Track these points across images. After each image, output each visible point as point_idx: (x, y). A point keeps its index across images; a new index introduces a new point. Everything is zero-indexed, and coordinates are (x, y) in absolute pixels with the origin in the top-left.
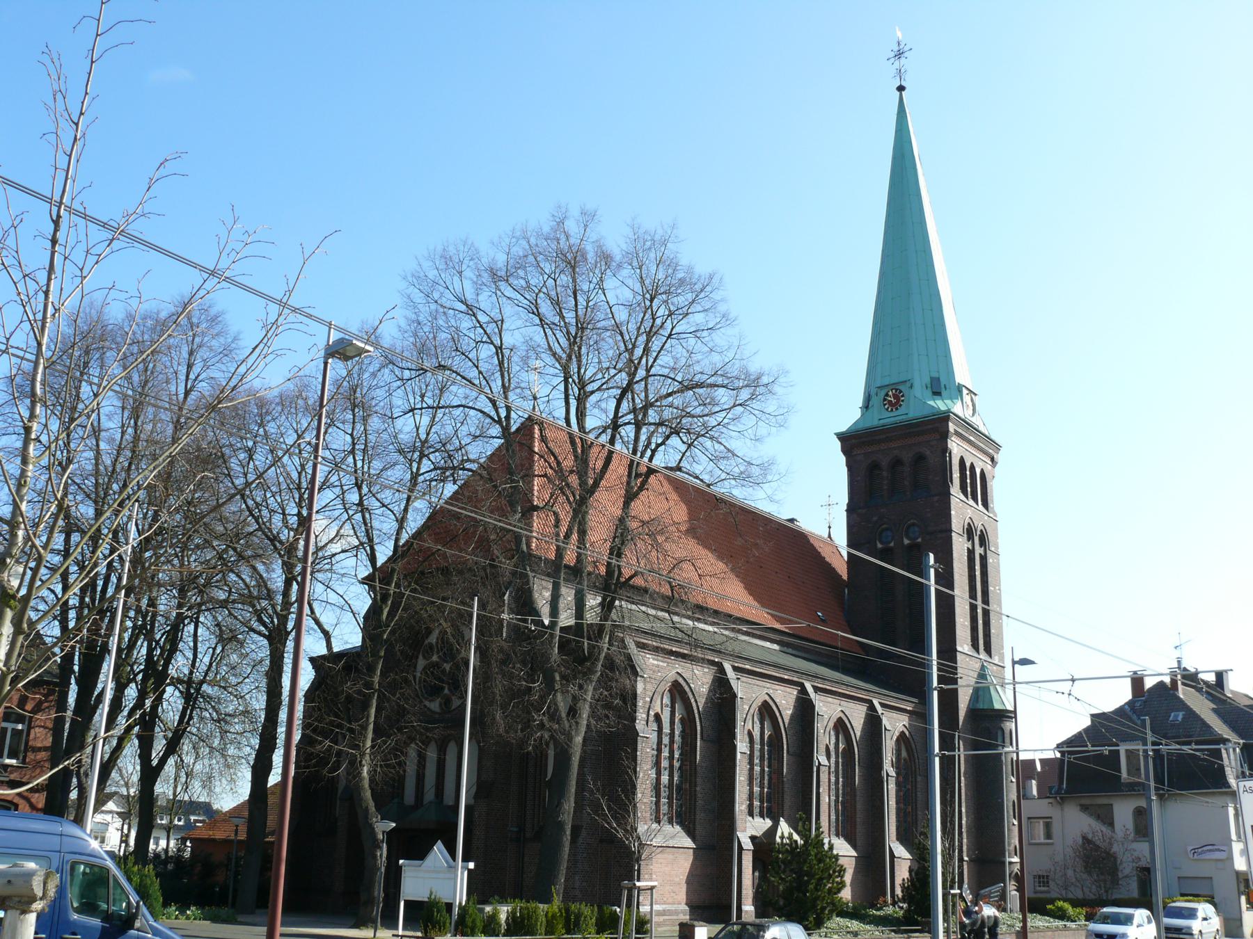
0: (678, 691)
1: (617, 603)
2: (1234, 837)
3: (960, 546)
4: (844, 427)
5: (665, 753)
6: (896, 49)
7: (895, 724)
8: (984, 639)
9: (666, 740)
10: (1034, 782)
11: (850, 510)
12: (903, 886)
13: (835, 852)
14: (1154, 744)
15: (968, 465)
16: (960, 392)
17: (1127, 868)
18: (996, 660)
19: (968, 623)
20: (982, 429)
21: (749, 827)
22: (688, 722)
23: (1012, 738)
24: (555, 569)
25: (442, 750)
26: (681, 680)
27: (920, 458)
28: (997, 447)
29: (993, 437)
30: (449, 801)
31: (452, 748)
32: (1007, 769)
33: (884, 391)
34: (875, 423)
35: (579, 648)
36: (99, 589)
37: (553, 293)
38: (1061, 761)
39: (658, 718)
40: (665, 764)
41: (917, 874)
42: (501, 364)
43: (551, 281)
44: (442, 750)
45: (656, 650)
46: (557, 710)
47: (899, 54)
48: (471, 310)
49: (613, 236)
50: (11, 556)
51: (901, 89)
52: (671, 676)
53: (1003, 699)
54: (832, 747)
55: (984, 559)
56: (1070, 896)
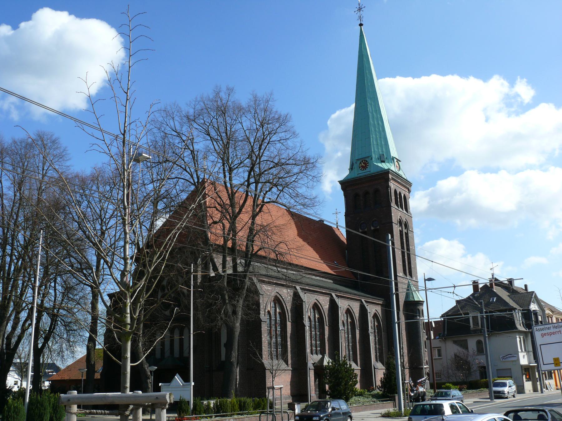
0: (278, 301)
1: (252, 263)
2: (520, 350)
3: (396, 229)
4: (342, 178)
5: (273, 328)
6: (358, 7)
7: (373, 309)
8: (409, 269)
9: (273, 323)
10: (432, 332)
11: (346, 215)
12: (381, 381)
13: (352, 368)
14: (486, 312)
15: (398, 193)
16: (394, 160)
17: (475, 368)
18: (414, 279)
19: (401, 263)
20: (403, 176)
21: (312, 359)
22: (283, 314)
23: (421, 313)
24: (222, 249)
25: (181, 334)
26: (278, 295)
27: (377, 191)
28: (410, 184)
29: (408, 180)
30: (185, 355)
31: (186, 331)
32: (421, 327)
33: (360, 160)
34: (356, 175)
35: (236, 283)
36: (7, 268)
37: (216, 126)
38: (444, 320)
39: (269, 312)
40: (273, 333)
41: (387, 375)
42: (194, 158)
43: (214, 120)
44: (181, 334)
45: (269, 283)
46: (228, 312)
47: (360, 9)
48: (179, 135)
49: (243, 98)
50: (126, 271)
51: (361, 25)
52: (273, 294)
53: (419, 296)
54: (345, 322)
55: (407, 234)
56: (451, 381)
